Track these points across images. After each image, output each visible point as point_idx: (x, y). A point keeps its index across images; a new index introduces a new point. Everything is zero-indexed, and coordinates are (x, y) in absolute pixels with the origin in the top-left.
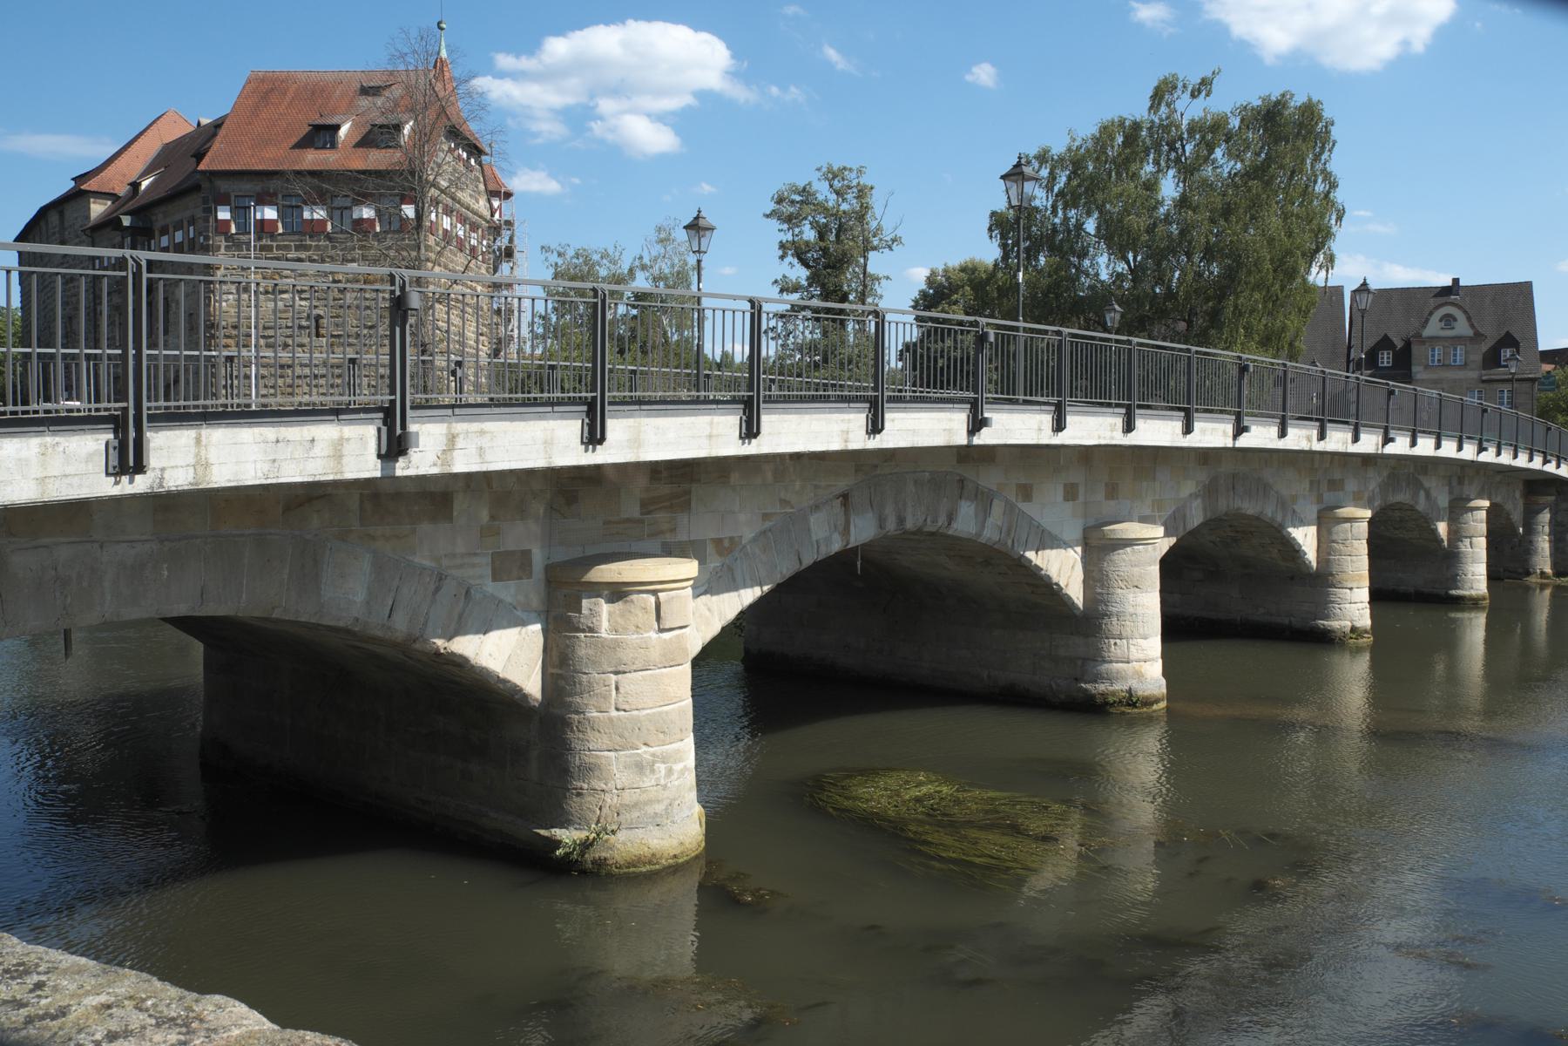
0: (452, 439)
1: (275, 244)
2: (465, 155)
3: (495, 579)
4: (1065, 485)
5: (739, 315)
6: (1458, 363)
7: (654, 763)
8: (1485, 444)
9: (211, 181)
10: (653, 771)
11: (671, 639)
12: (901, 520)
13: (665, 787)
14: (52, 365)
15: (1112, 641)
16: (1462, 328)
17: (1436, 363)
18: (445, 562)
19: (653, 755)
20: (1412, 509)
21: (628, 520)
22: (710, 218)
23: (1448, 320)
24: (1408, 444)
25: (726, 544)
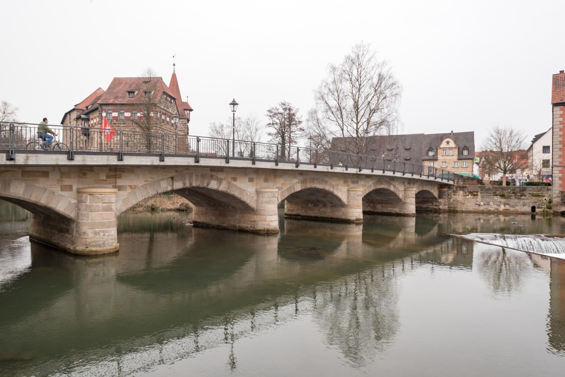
1: (117, 123)
2: (170, 100)
3: (61, 190)
4: (249, 178)
5: (194, 140)
6: (451, 154)
9: (101, 106)
10: (99, 234)
12: (191, 184)
13: (103, 238)
16: (452, 144)
17: (445, 155)
18: (46, 186)
19: (99, 231)
20: (389, 190)
23: (448, 143)
25: (133, 187)
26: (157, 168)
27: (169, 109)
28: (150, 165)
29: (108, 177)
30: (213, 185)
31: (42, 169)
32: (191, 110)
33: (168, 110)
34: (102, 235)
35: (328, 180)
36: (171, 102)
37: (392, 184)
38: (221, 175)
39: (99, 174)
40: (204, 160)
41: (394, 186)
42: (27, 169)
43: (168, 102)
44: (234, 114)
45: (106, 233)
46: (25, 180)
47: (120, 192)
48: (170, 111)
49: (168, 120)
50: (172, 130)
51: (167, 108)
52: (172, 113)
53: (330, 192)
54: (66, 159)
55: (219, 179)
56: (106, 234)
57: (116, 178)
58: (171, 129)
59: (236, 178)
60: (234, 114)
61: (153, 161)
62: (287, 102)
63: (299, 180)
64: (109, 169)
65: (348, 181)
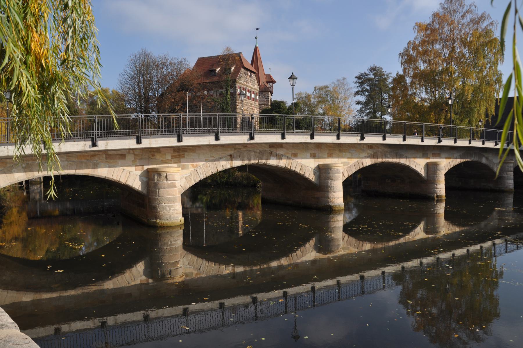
0: (107, 144)
4: (311, 154)
7: (166, 207)
8: (498, 142)
10: (166, 209)
11: (170, 183)
13: (169, 212)
14: (94, 124)
15: (325, 193)
21: (168, 160)
22: (296, 75)
24: (468, 143)
26: (216, 147)
27: (249, 83)
28: (207, 145)
29: (172, 157)
30: (273, 162)
31: (119, 152)
32: (274, 82)
33: (248, 84)
34: (168, 209)
35: (403, 153)
36: (251, 76)
37: (484, 156)
38: (281, 152)
39: (165, 155)
40: (260, 137)
41: (487, 159)
42: (110, 153)
43: (248, 76)
44: (293, 88)
45: (172, 207)
46: (108, 162)
47: (183, 170)
48: (251, 85)
49: (248, 95)
50: (253, 104)
51: (247, 82)
52: (252, 87)
53: (406, 166)
54: (214, 140)
55: (279, 155)
56: (171, 208)
57: (179, 157)
58: (251, 104)
59: (297, 154)
60: (293, 88)
61: (210, 141)
62: (377, 66)
63: (368, 153)
64: (174, 150)
65: (427, 154)
